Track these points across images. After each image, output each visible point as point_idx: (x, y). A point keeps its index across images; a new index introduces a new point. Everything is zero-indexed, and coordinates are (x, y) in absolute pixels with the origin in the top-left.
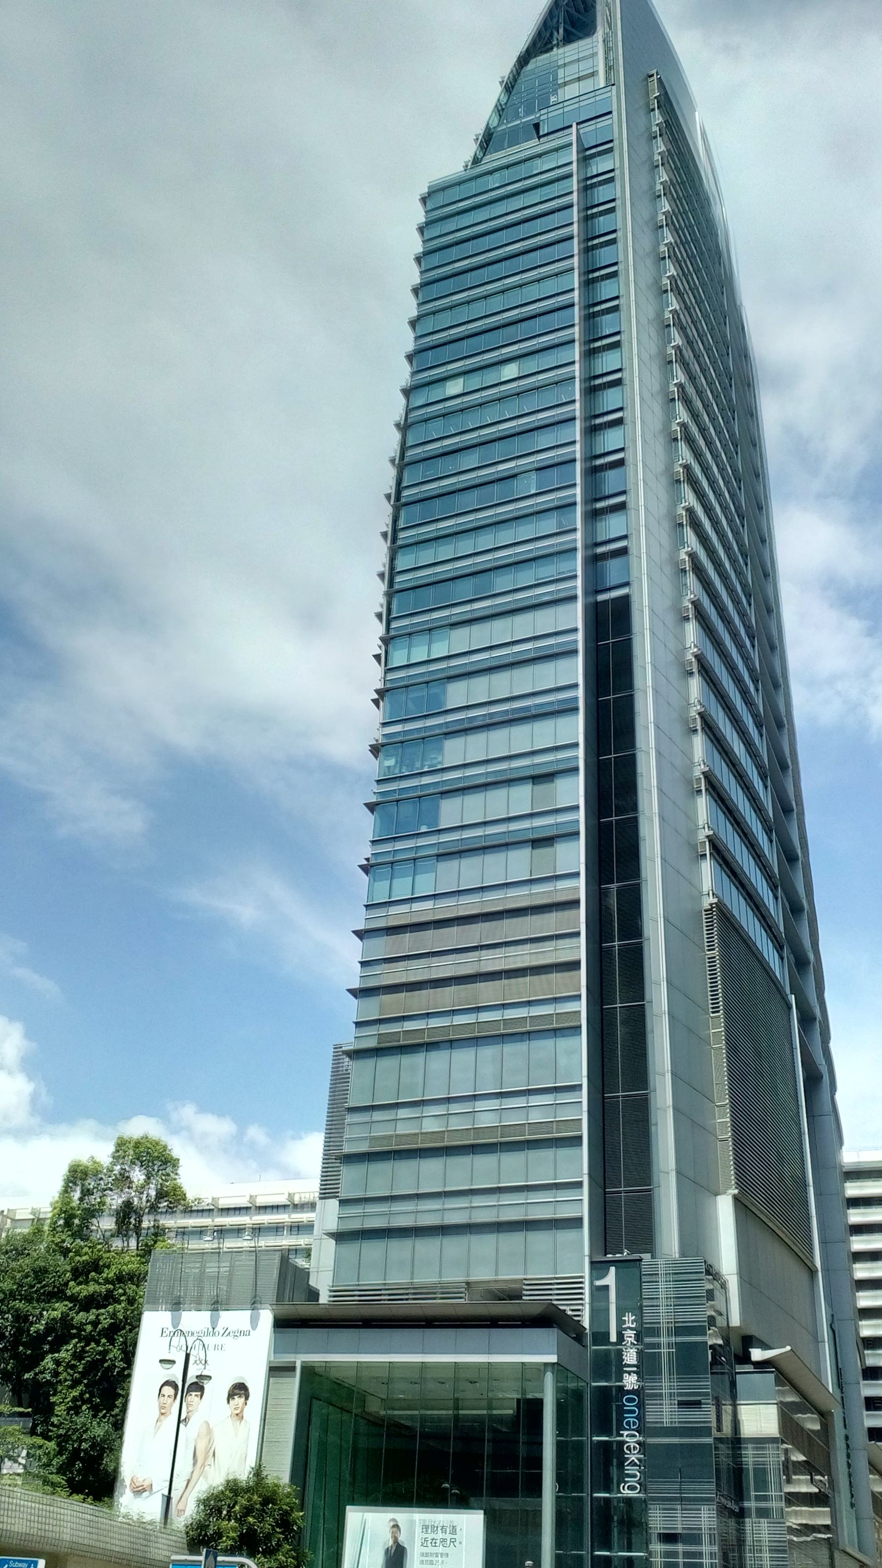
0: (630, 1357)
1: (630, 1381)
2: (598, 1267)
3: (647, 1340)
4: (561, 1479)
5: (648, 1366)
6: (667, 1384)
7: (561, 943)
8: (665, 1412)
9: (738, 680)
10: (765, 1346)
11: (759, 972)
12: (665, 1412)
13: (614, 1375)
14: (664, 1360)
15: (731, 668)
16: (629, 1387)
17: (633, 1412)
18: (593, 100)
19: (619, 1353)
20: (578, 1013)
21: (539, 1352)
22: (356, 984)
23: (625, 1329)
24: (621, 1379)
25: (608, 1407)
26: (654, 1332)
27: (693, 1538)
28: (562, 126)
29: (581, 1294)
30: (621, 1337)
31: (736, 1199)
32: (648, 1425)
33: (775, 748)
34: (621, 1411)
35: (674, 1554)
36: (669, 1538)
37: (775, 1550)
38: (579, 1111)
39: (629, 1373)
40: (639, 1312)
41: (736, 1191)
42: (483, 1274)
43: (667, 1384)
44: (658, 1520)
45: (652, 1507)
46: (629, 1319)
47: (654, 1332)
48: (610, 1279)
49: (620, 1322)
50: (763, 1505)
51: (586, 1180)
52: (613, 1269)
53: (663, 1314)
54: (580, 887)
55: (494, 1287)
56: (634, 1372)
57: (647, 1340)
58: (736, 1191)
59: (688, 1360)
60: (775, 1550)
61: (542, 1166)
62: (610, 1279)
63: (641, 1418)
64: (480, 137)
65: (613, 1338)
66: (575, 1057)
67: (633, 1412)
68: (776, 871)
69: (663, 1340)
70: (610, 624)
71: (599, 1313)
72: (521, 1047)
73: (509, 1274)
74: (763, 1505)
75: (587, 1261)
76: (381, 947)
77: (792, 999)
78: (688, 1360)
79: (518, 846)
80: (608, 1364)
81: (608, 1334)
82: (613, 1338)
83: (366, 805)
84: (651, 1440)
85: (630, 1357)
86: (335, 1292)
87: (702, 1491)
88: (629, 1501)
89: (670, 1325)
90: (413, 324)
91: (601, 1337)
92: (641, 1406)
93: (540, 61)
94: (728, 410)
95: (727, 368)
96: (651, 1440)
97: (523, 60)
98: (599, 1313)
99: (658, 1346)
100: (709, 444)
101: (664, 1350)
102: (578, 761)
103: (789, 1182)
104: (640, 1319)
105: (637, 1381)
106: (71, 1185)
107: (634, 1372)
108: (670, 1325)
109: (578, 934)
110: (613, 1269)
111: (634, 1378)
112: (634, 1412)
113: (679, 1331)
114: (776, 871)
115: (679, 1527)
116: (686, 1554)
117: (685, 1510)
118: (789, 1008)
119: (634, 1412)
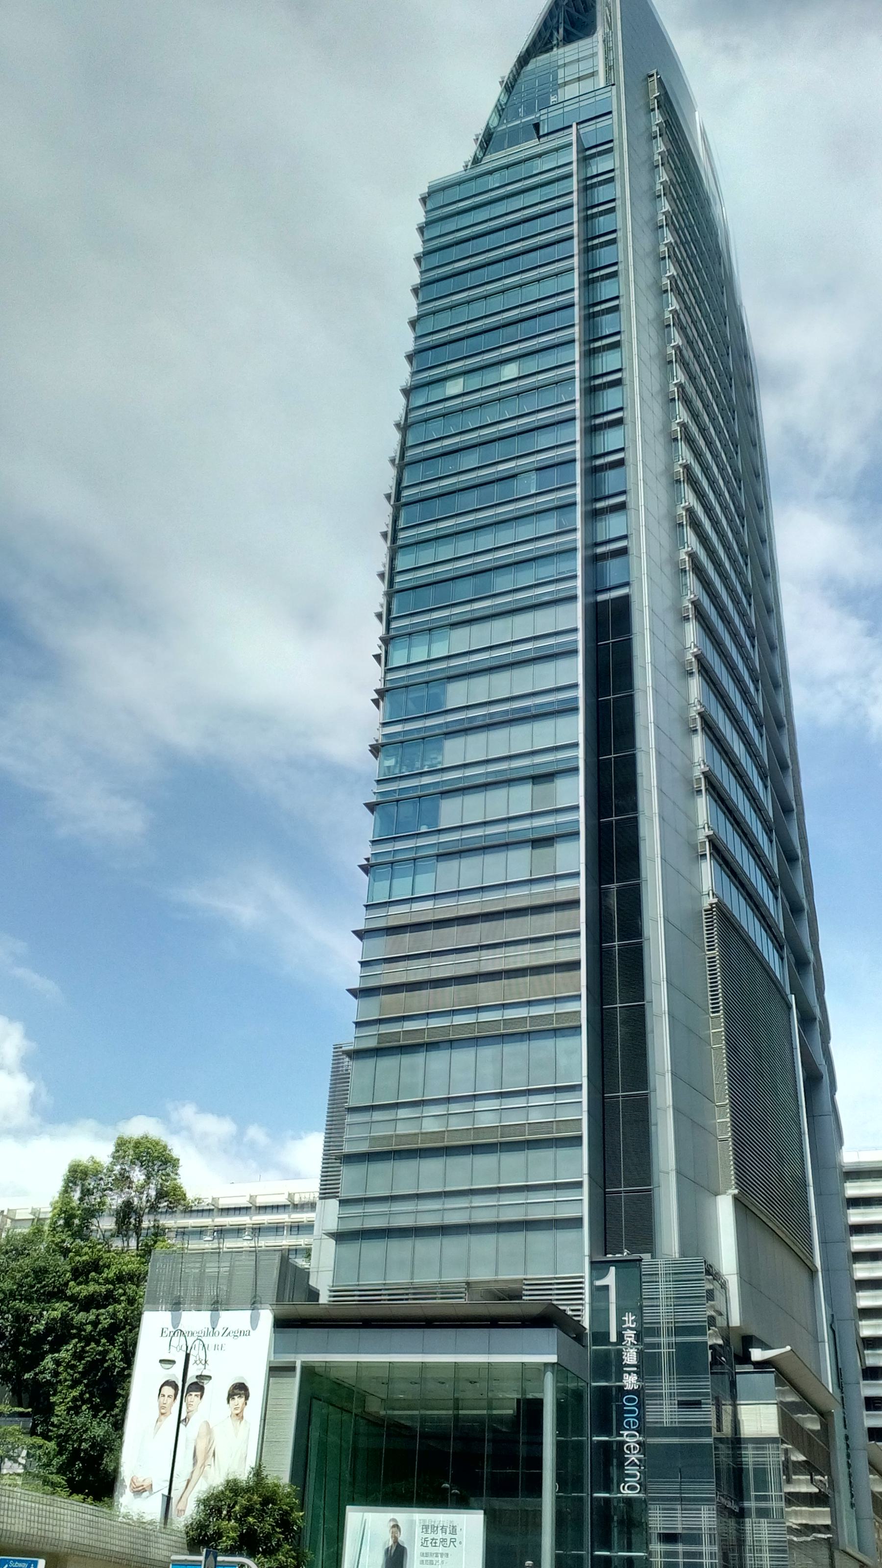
0: (630, 1357)
1: (630, 1381)
2: (598, 1267)
3: (647, 1340)
4: (561, 1479)
5: (648, 1366)
6: (667, 1384)
7: (561, 943)
8: (665, 1412)
9: (738, 680)
10: (765, 1346)
11: (759, 972)
12: (665, 1412)
13: (614, 1375)
14: (664, 1360)
15: (731, 668)
16: (629, 1387)
17: (633, 1412)
18: (593, 100)
19: (619, 1353)
20: (578, 1013)
21: (539, 1352)
22: (356, 984)
23: (625, 1329)
24: (621, 1379)
25: (608, 1407)
26: (654, 1332)
27: (693, 1538)
28: (562, 126)
29: (581, 1294)
30: (621, 1337)
31: (736, 1199)
32: (648, 1425)
33: (775, 748)
34: (621, 1411)
35: (674, 1554)
36: (669, 1538)
37: (775, 1550)
38: (579, 1111)
39: (629, 1373)
40: (639, 1312)
41: (736, 1191)
42: (483, 1274)
43: (667, 1384)
44: (658, 1520)
45: (652, 1507)
46: (629, 1319)
47: (654, 1332)
48: (610, 1279)
49: (620, 1322)
50: (763, 1505)
51: (586, 1180)
52: (613, 1269)
53: (663, 1314)
54: (580, 887)
55: (494, 1287)
56: (634, 1372)
57: (647, 1340)
58: (736, 1191)
59: (688, 1360)
60: (775, 1550)
61: (542, 1166)
62: (610, 1279)
63: (641, 1418)
64: (480, 137)
65: (613, 1338)
66: (575, 1057)
67: (633, 1412)
68: (776, 871)
69: (663, 1340)
70: (610, 624)
71: (599, 1313)
72: (521, 1047)
73: (509, 1274)
74: (763, 1505)
75: (587, 1261)
76: (381, 947)
77: (792, 999)
78: (688, 1360)
79: (518, 846)
80: (608, 1364)
81: (608, 1334)
82: (613, 1338)
83: (366, 805)
84: (651, 1440)
85: (630, 1357)
86: (335, 1292)
87: (702, 1491)
88: (629, 1501)
89: (670, 1325)
90: (413, 324)
91: (601, 1337)
92: (641, 1406)
93: (540, 61)
94: (728, 410)
95: (727, 368)
96: (651, 1440)
97: (523, 60)
98: (599, 1313)
99: (658, 1346)
100: (709, 444)
101: (664, 1350)
102: (578, 761)
103: (789, 1182)
104: (640, 1319)
105: (637, 1381)
106: (71, 1185)
107: (634, 1372)
108: (670, 1325)
109: (578, 934)
110: (613, 1269)
111: (634, 1378)
112: (634, 1412)
113: (679, 1331)
114: (776, 871)
115: (679, 1527)
116: (686, 1554)
117: (685, 1510)
118: (789, 1008)
119: (634, 1412)
